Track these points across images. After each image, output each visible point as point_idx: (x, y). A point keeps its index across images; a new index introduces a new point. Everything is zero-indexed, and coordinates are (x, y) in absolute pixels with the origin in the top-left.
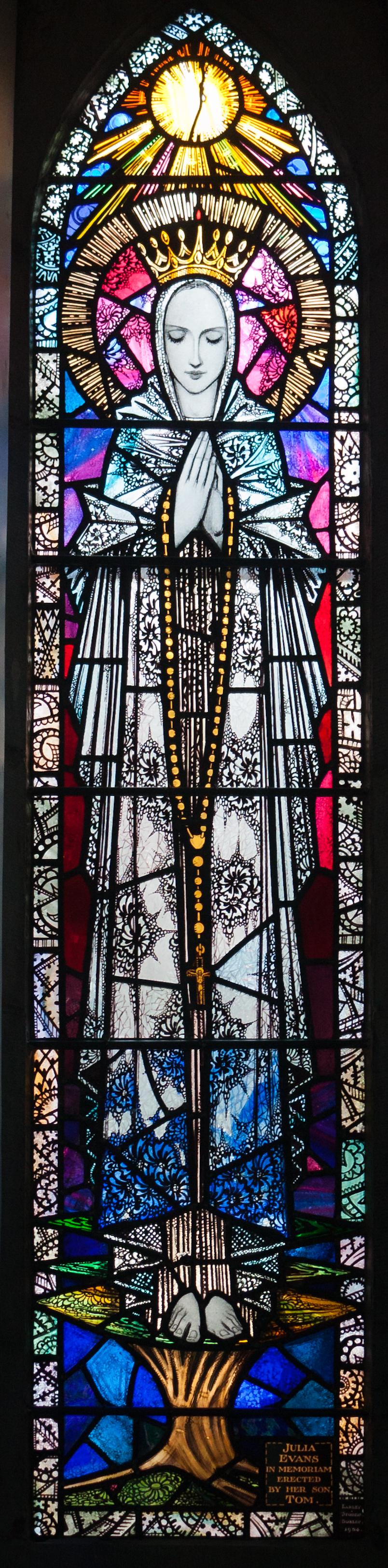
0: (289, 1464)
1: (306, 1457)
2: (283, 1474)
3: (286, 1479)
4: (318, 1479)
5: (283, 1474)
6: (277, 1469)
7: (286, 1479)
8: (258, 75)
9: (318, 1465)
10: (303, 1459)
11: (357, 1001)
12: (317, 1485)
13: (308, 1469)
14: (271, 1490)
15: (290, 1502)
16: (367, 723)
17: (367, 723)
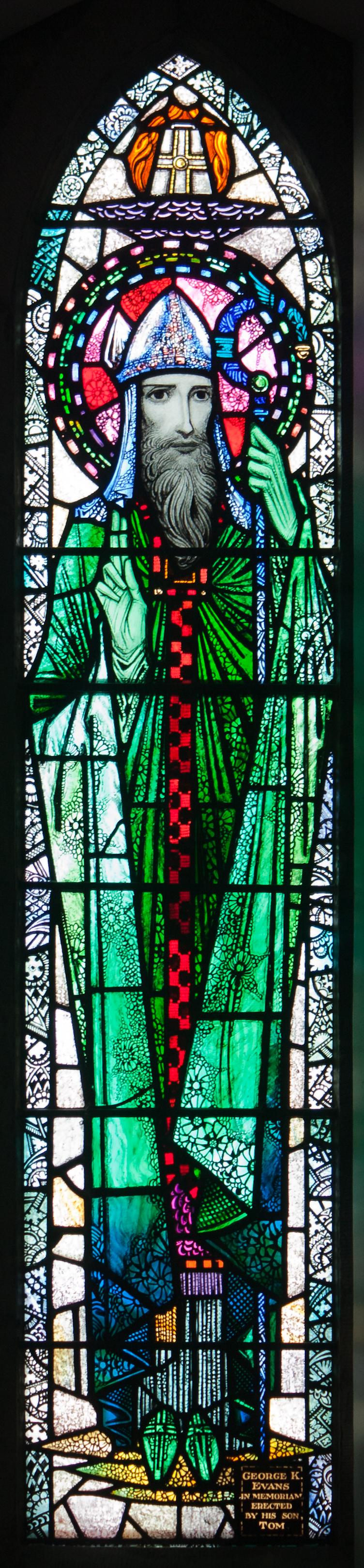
0: (262, 1491)
1: (277, 1485)
2: (256, 1501)
3: (260, 1506)
4: (289, 1506)
5: (256, 1501)
6: (251, 1496)
7: (260, 1506)
8: (184, 637)
9: (289, 1492)
10: (275, 1486)
11: (238, 527)
12: (287, 1511)
14: (248, 1515)
15: (263, 1528)
16: (337, 310)
17: (337, 310)
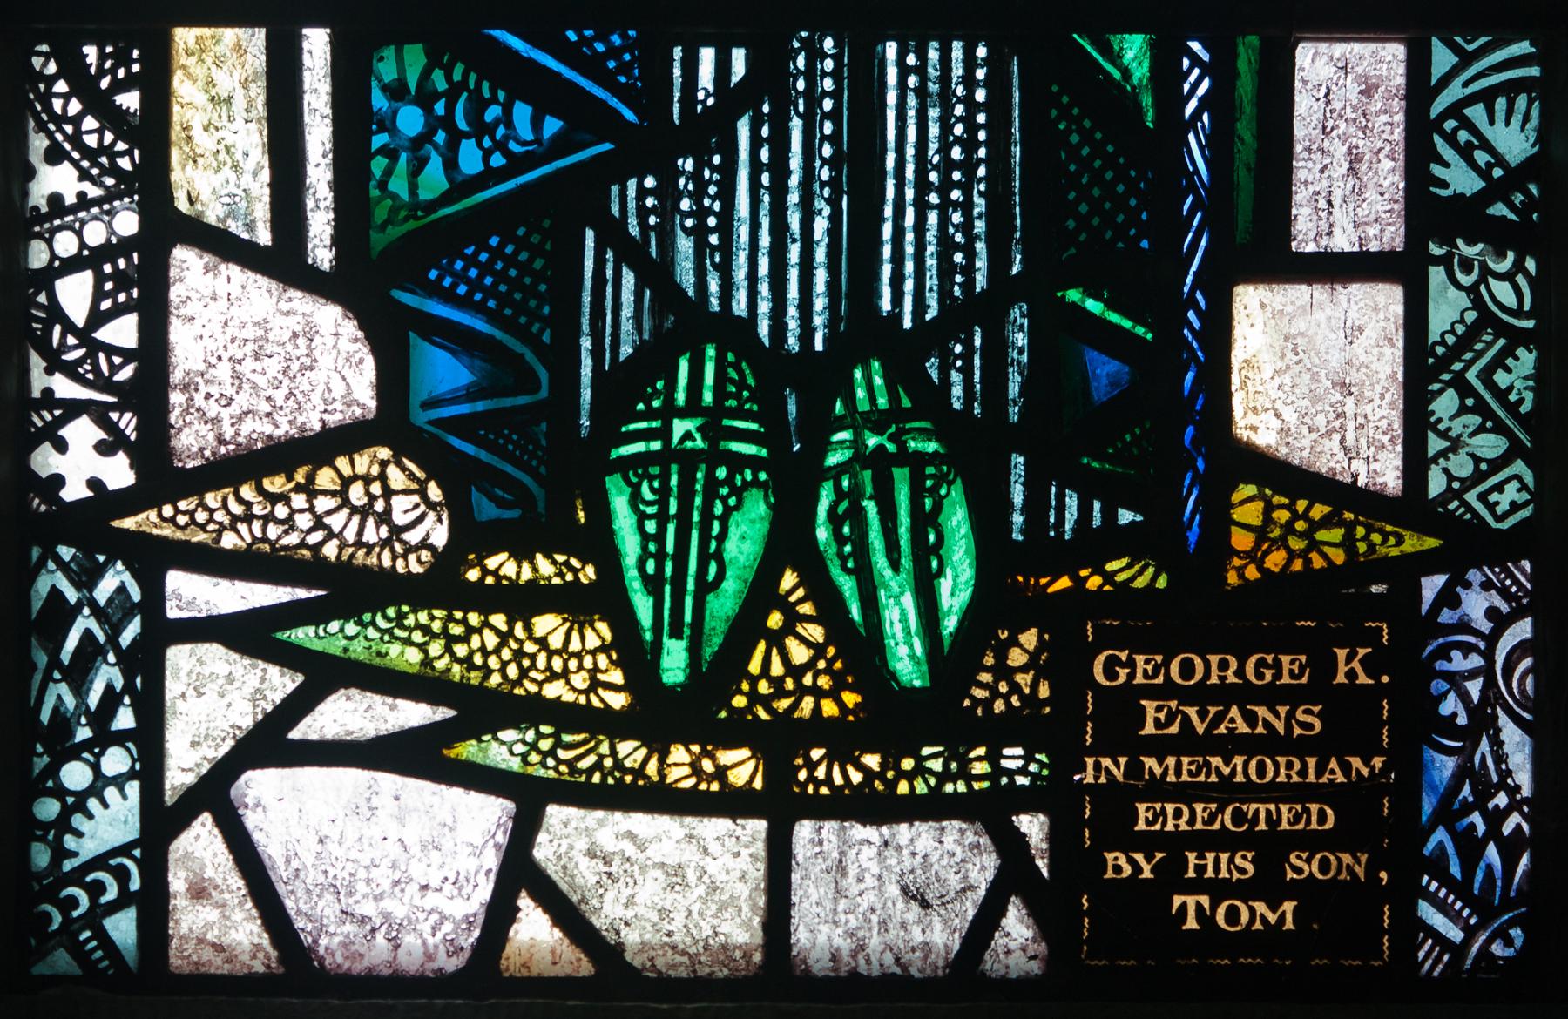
0: (1187, 742)
2: (1158, 790)
5: (1158, 790)
6: (1134, 769)
7: (1175, 819)
10: (1251, 719)
12: (1310, 842)
13: (1282, 770)
15: (1191, 924)
